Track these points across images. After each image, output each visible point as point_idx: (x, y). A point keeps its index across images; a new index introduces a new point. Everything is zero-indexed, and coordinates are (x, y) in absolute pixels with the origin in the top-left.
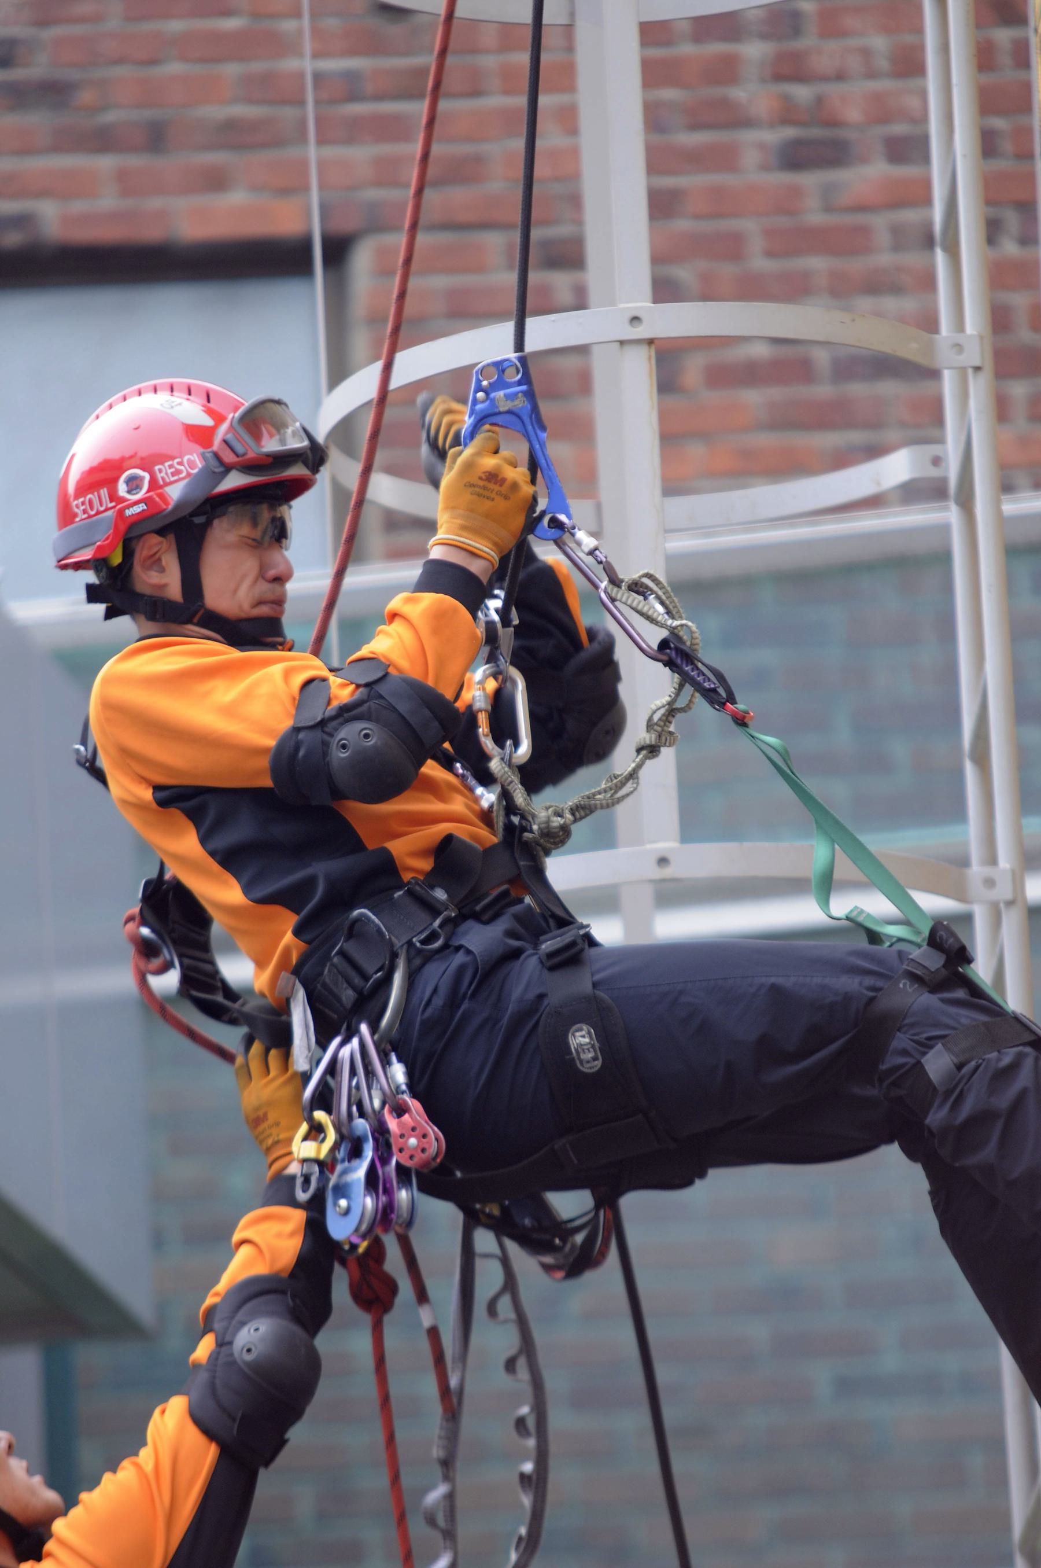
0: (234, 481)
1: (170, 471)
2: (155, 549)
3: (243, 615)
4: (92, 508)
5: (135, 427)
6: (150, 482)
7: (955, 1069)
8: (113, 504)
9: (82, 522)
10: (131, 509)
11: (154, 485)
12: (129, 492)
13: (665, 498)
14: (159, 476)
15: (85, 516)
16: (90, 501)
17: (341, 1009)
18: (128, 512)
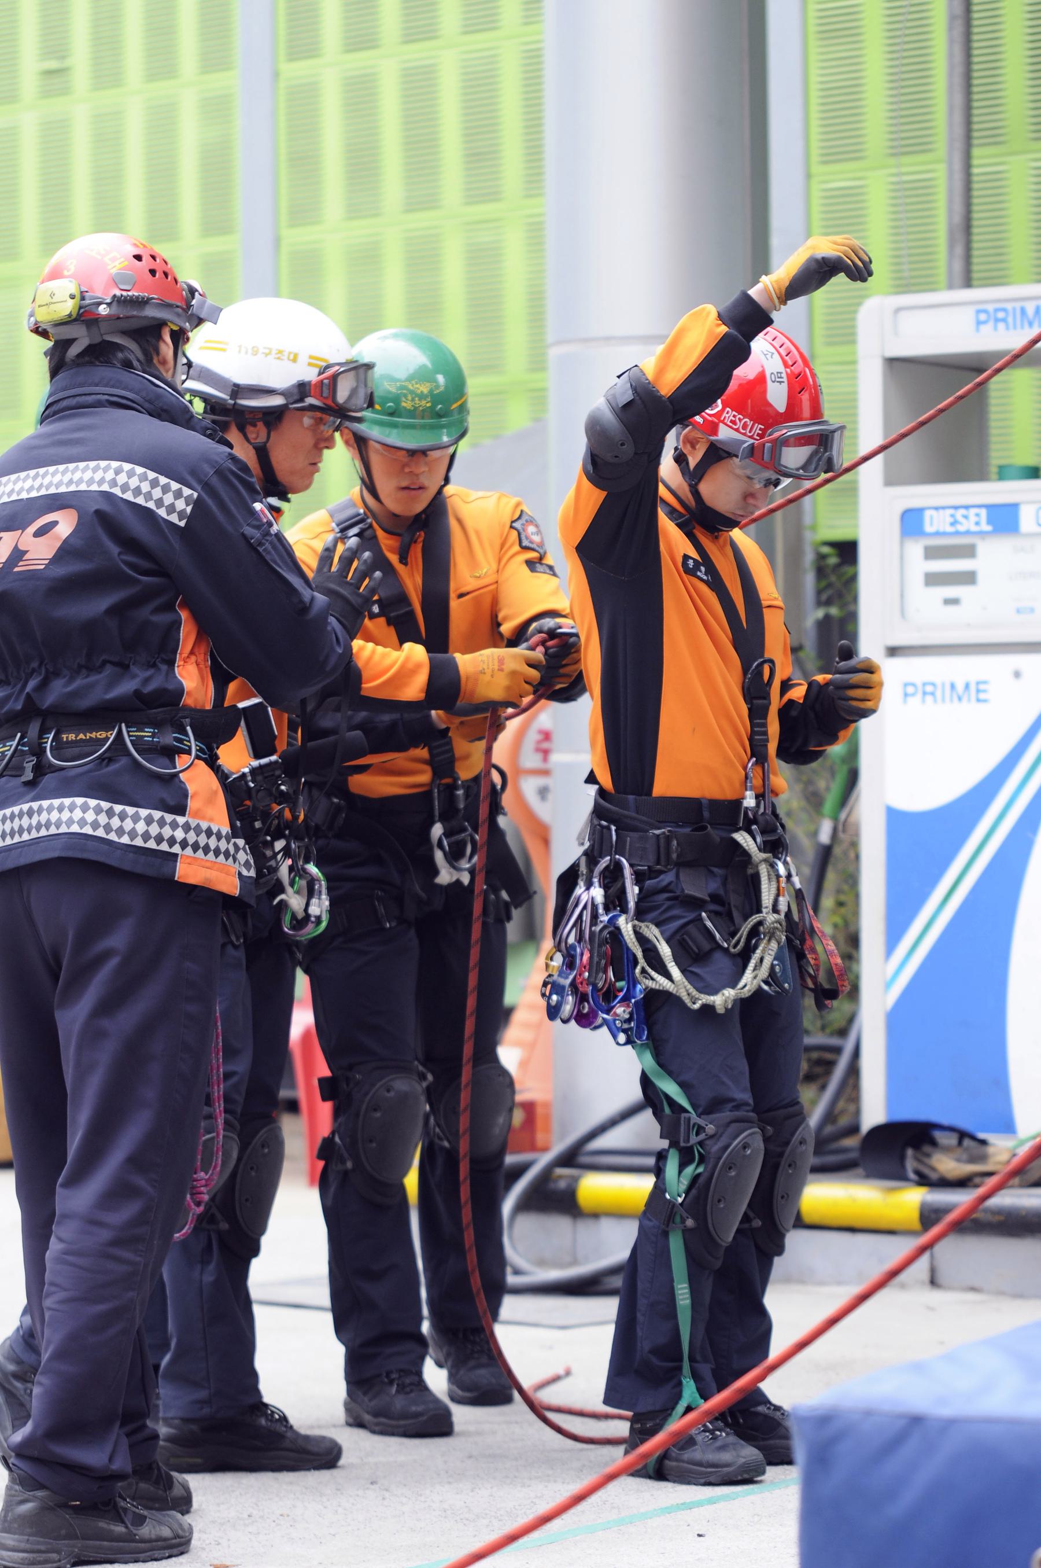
7: (915, 1215)
8: (758, 438)
13: (457, 1428)
14: (725, 414)
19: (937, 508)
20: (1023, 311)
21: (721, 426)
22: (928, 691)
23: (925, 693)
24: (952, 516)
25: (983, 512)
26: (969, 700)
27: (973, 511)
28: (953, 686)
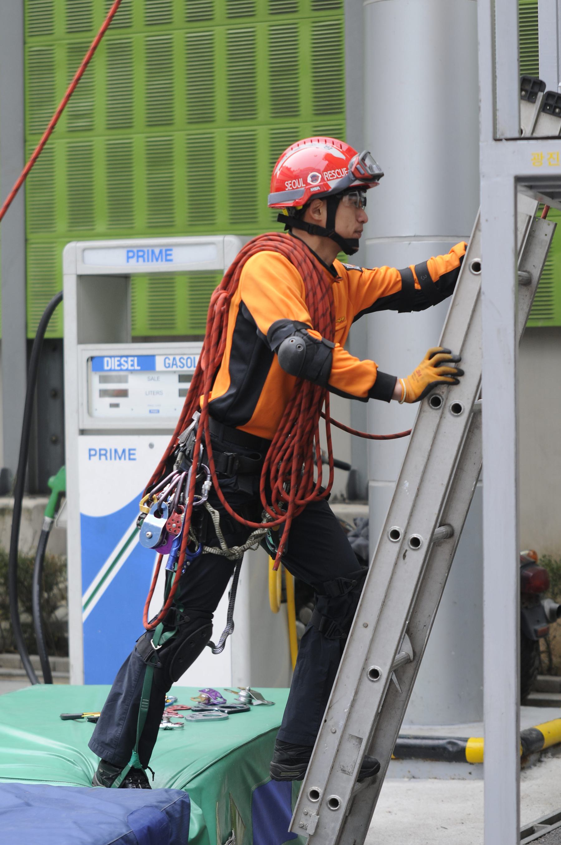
0: (357, 183)
1: (330, 175)
2: (318, 205)
3: (349, 237)
4: (294, 186)
5: (315, 155)
6: (321, 179)
8: (305, 185)
9: (289, 191)
10: (313, 188)
11: (323, 179)
12: (312, 181)
14: (325, 177)
15: (291, 188)
16: (294, 182)
17: (206, 417)
18: (312, 190)
19: (111, 357)
20: (153, 252)
21: (329, 183)
22: (102, 453)
23: (100, 455)
24: (118, 361)
25: (136, 359)
26: (125, 459)
27: (130, 359)
28: (116, 451)
